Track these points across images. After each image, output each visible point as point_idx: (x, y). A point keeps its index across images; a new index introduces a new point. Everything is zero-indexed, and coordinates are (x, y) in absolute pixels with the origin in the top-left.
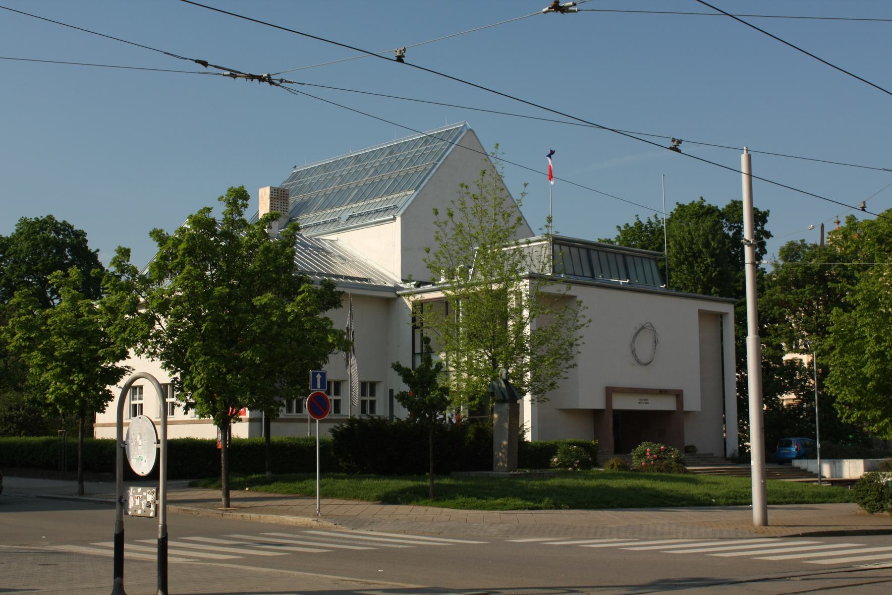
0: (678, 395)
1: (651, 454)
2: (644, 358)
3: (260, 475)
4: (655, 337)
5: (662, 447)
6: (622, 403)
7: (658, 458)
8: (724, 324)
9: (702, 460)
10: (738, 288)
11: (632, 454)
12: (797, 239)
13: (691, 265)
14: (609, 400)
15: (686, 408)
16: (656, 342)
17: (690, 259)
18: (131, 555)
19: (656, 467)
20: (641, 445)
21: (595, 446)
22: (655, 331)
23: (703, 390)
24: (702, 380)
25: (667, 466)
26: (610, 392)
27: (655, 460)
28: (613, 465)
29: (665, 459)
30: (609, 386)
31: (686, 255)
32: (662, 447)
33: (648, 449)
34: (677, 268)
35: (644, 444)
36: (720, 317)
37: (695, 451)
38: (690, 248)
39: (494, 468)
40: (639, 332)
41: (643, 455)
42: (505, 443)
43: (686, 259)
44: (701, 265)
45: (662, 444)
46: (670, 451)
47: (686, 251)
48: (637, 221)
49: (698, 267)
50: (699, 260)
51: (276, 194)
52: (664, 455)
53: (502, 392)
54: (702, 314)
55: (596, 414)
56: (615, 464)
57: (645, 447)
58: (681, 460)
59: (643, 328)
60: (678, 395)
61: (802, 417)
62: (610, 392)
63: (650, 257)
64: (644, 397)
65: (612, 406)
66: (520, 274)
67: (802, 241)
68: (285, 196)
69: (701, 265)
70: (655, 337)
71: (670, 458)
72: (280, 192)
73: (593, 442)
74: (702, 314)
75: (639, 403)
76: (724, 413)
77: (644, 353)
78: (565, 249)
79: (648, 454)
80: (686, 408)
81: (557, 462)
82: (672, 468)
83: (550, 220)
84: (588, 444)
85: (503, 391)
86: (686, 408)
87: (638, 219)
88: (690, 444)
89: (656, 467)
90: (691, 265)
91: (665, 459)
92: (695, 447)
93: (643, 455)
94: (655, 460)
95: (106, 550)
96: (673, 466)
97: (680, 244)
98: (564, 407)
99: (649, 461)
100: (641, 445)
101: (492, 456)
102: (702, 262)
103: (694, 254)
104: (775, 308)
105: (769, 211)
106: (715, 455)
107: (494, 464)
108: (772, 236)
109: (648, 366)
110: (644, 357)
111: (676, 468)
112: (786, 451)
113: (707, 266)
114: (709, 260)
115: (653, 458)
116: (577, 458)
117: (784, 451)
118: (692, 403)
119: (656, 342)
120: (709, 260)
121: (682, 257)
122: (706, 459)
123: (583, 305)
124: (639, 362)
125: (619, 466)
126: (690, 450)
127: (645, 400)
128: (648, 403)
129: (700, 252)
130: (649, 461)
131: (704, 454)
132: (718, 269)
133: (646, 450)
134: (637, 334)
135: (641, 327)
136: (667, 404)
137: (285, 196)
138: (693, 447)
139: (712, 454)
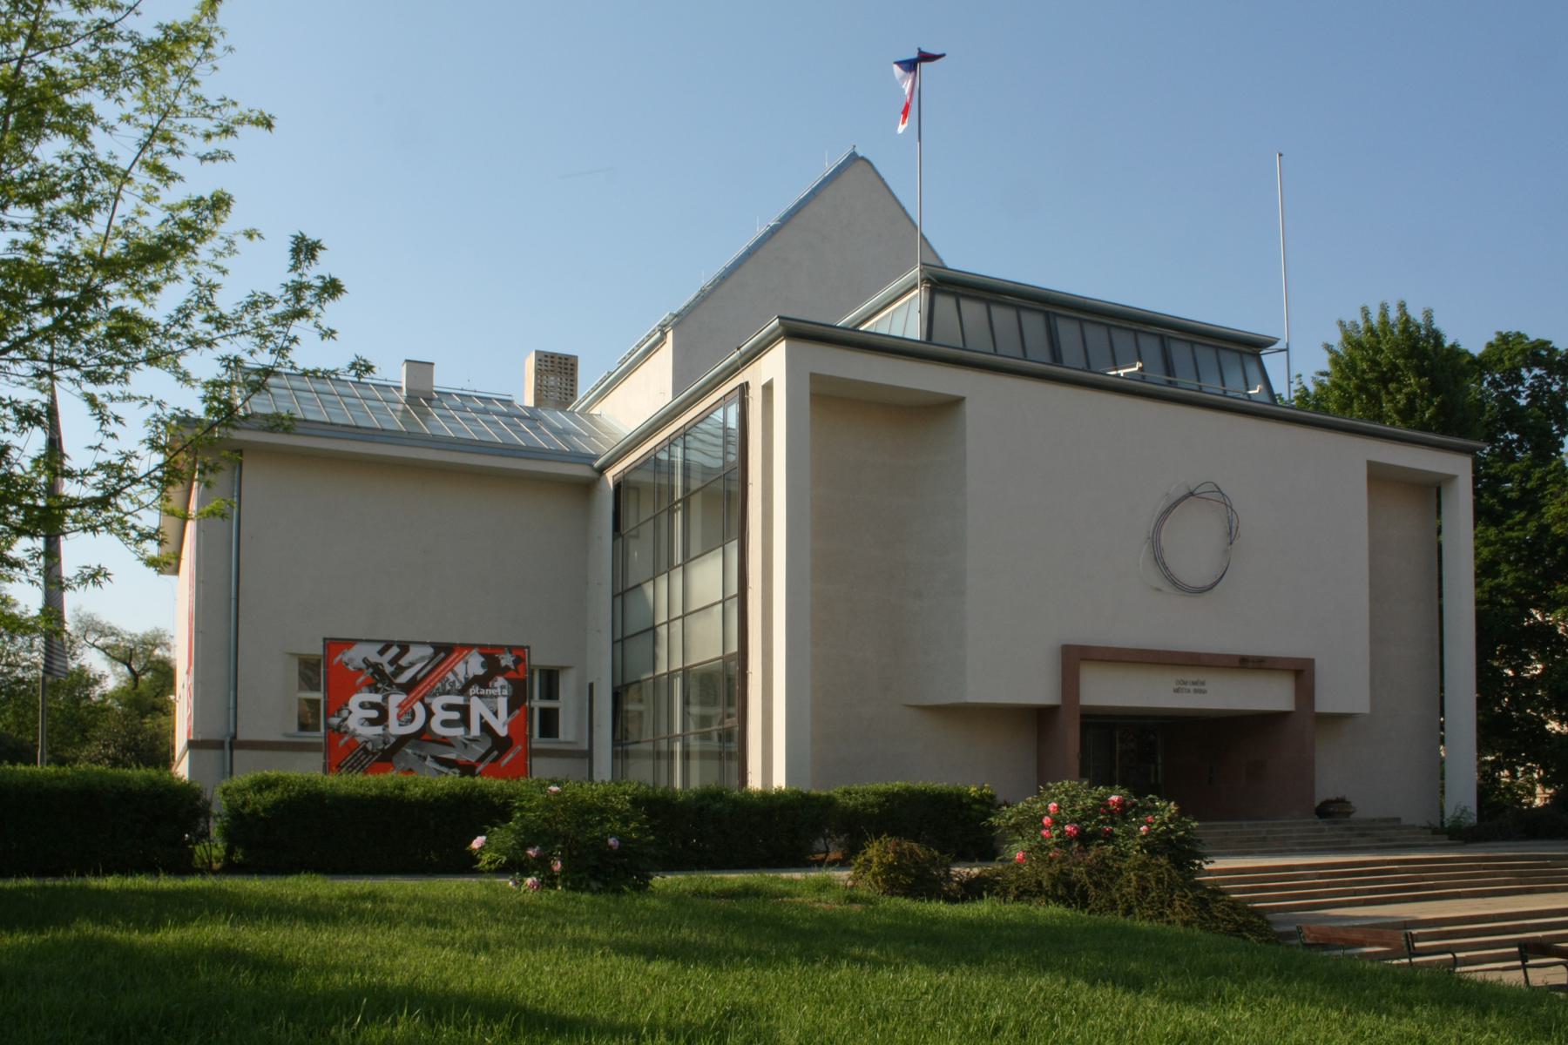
0: (1301, 673)
1: (1057, 822)
3: (117, 936)
4: (1230, 522)
9: (1363, 835)
10: (1509, 495)
15: (1324, 704)
16: (1231, 534)
17: (1373, 387)
22: (1228, 506)
24: (1376, 639)
26: (1074, 659)
36: (1433, 490)
37: (1348, 814)
43: (1361, 388)
47: (1364, 372)
50: (1392, 386)
51: (549, 364)
55: (1040, 719)
60: (1301, 673)
62: (1074, 659)
64: (1191, 676)
65: (1077, 695)
68: (569, 367)
70: (1230, 522)
72: (557, 361)
74: (1379, 476)
75: (1176, 691)
76: (1442, 714)
77: (1194, 563)
79: (1046, 820)
80: (1325, 703)
86: (1325, 703)
88: (1332, 796)
90: (1375, 399)
98: (927, 703)
109: (1207, 595)
113: (1411, 398)
119: (1231, 534)
121: (1354, 381)
124: (1175, 583)
127: (1195, 683)
128: (1204, 692)
129: (1395, 367)
132: (1436, 401)
134: (1166, 513)
135: (1187, 491)
136: (1273, 695)
137: (569, 367)
138: (1341, 801)
139: (1398, 819)
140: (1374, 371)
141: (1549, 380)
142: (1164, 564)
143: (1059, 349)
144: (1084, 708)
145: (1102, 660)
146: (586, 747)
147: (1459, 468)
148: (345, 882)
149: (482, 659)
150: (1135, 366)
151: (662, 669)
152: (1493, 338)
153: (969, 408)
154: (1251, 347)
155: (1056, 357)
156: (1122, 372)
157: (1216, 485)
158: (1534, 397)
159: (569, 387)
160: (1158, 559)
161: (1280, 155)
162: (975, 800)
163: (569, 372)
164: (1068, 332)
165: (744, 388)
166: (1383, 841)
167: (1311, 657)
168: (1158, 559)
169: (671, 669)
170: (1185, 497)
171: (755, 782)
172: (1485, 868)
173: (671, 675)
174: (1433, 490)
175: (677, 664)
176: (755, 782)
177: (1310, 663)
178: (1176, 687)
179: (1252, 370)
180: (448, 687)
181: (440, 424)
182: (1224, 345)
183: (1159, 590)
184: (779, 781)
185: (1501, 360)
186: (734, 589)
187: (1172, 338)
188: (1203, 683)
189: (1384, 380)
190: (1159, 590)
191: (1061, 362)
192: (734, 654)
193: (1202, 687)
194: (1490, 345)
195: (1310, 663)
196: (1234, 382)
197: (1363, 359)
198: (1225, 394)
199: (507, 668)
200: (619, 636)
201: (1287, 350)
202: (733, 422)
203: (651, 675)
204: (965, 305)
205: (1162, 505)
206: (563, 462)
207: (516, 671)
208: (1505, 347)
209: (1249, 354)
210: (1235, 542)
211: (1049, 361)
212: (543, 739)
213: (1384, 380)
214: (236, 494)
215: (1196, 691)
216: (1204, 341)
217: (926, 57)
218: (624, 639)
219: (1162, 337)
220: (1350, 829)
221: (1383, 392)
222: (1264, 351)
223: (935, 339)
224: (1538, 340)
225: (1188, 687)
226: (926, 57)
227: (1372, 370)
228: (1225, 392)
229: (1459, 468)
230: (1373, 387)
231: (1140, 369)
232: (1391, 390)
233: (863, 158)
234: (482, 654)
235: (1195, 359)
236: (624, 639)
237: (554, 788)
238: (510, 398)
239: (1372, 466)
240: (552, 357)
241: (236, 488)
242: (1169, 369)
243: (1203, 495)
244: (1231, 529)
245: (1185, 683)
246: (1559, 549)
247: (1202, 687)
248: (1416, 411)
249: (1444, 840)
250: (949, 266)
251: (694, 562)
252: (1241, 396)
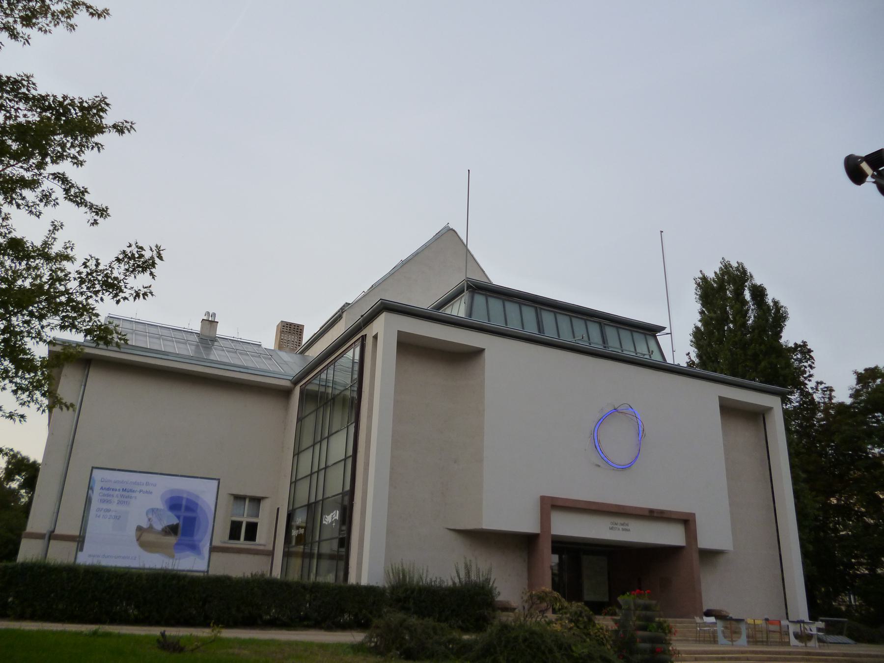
0: (687, 522)
14: (545, 520)
16: (641, 434)
48: (689, 360)
51: (288, 328)
60: (687, 522)
61: (855, 424)
64: (619, 521)
66: (23, 95)
74: (728, 409)
75: (611, 529)
77: (620, 450)
80: (705, 541)
87: (690, 359)
95: (873, 653)
108: (856, 372)
135: (612, 408)
136: (672, 536)
137: (299, 331)
144: (553, 536)
146: (271, 548)
147: (773, 402)
148: (111, 631)
153: (487, 354)
154: (651, 331)
155: (540, 329)
159: (298, 342)
160: (597, 446)
163: (299, 333)
165: (364, 338)
167: (693, 512)
168: (597, 446)
169: (317, 500)
170: (610, 414)
176: (352, 580)
178: (611, 526)
179: (652, 344)
181: (216, 355)
182: (636, 330)
183: (599, 466)
186: (350, 452)
187: (605, 324)
188: (627, 525)
190: (599, 466)
192: (348, 491)
196: (642, 349)
200: (294, 479)
201: (671, 334)
202: (357, 357)
206: (157, 350)
209: (650, 335)
212: (232, 541)
214: (83, 384)
215: (623, 530)
216: (640, 331)
218: (295, 482)
222: (658, 334)
225: (618, 526)
233: (452, 230)
236: (295, 482)
238: (260, 344)
239: (721, 398)
240: (290, 325)
242: (604, 341)
243: (625, 411)
250: (494, 283)
251: (334, 436)
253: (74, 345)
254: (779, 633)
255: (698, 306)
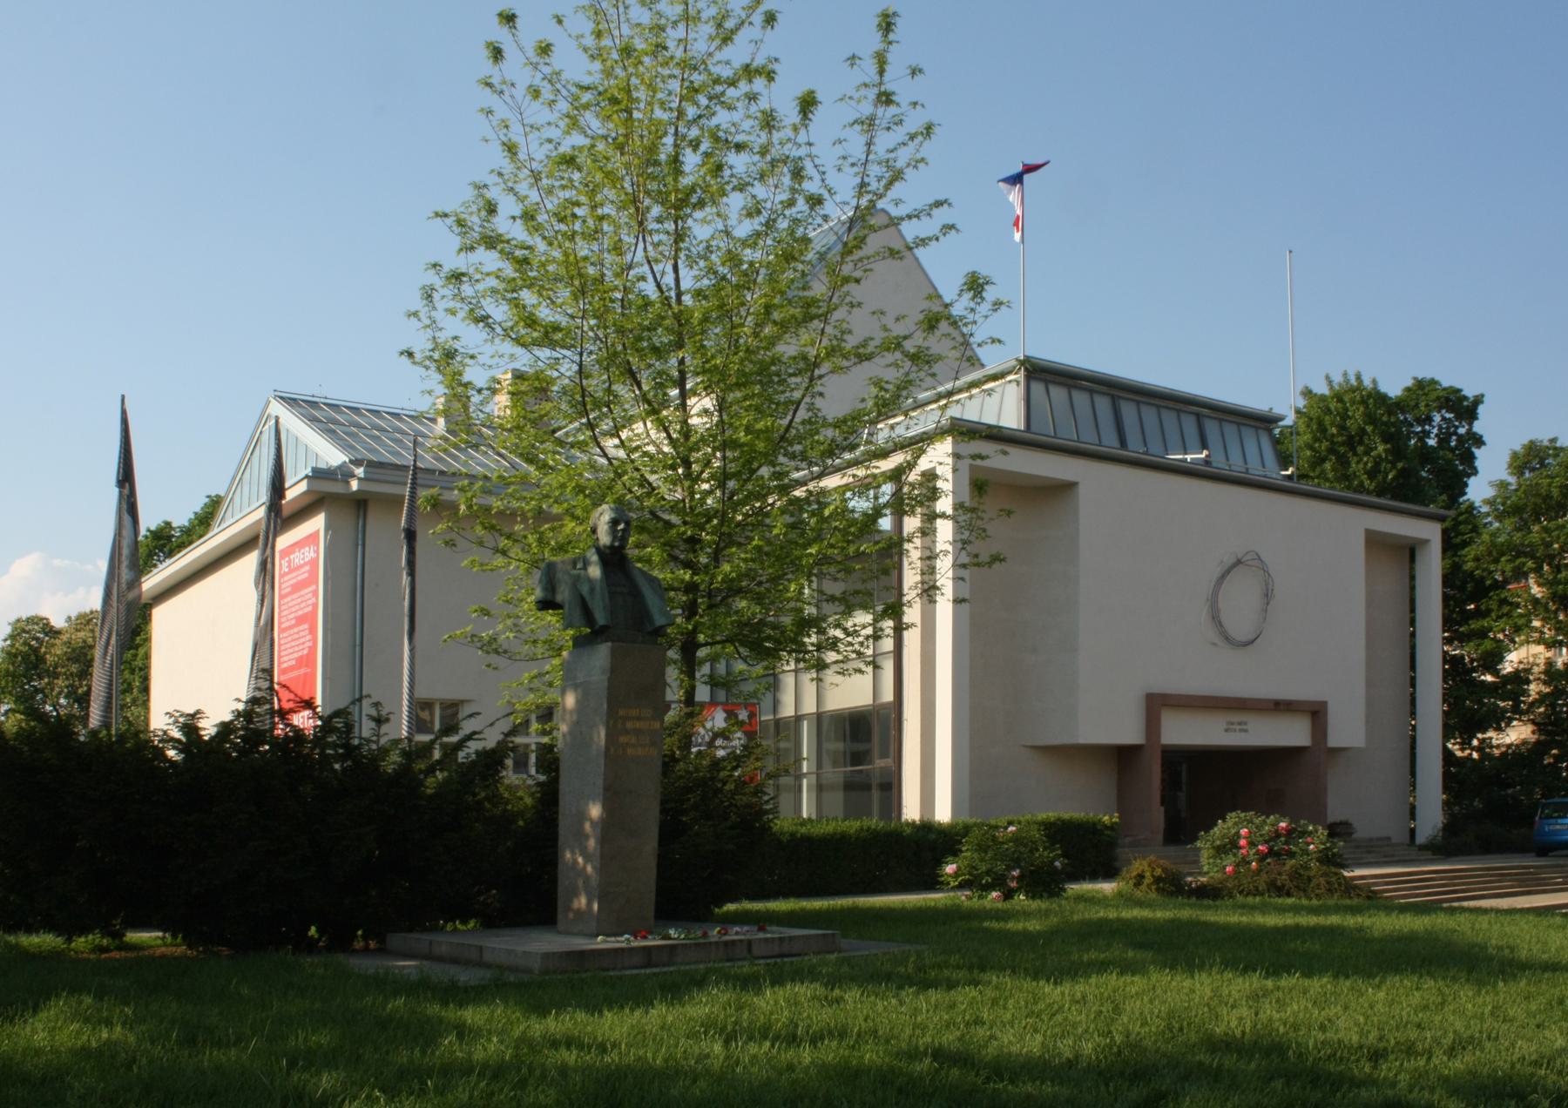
0: (1317, 713)
1: (1252, 844)
2: (1240, 630)
4: (1267, 585)
5: (1283, 825)
6: (1183, 731)
7: (1271, 853)
8: (1418, 558)
9: (1369, 852)
11: (1198, 844)
12: (1543, 436)
13: (1343, 462)
14: (1152, 724)
16: (1268, 595)
17: (1342, 449)
18: (903, 901)
19: (1264, 877)
20: (1224, 820)
21: (1112, 827)
23: (1370, 704)
25: (1295, 875)
26: (1156, 705)
27: (1262, 858)
28: (1141, 877)
29: (1291, 855)
30: (1151, 691)
31: (1332, 443)
32: (1283, 825)
33: (1244, 831)
34: (1314, 471)
35: (1232, 817)
36: (1410, 551)
37: (1351, 834)
38: (1342, 428)
39: (560, 916)
40: (1228, 571)
41: (1229, 846)
42: (595, 811)
43: (1331, 451)
44: (1365, 459)
45: (1283, 815)
46: (1304, 833)
47: (1333, 435)
49: (1358, 462)
52: (1287, 843)
53: (583, 599)
54: (1375, 541)
55: (1123, 757)
56: (1148, 874)
57: (1236, 825)
58: (1334, 855)
59: (1239, 562)
60: (1317, 713)
62: (1156, 705)
63: (1258, 424)
64: (1236, 717)
65: (1159, 736)
67: (1553, 440)
69: (1365, 459)
70: (1267, 585)
71: (1306, 852)
73: (1106, 818)
74: (1375, 541)
75: (1227, 730)
77: (1240, 621)
78: (1059, 393)
79: (1242, 842)
80: (1334, 741)
81: (956, 875)
82: (1309, 879)
83: (887, 24)
84: (1094, 824)
85: (585, 590)
86: (1334, 741)
89: (1264, 877)
90: (1343, 462)
91: (1291, 855)
92: (1351, 825)
93: (1229, 846)
94: (1262, 858)
96: (1312, 873)
97: (1320, 423)
99: (1245, 862)
100: (1224, 820)
101: (555, 865)
102: (1367, 453)
103: (1350, 437)
104: (1503, 559)
105: (1483, 396)
106: (1394, 841)
107: (560, 903)
109: (1250, 647)
110: (1240, 626)
111: (1322, 880)
112: (1558, 827)
114: (1381, 448)
115: (1258, 852)
116: (1016, 862)
117: (1551, 827)
118: (1347, 730)
119: (1268, 595)
120: (1381, 448)
121: (1325, 444)
122: (1377, 851)
123: (990, 293)
124: (1227, 638)
125: (1157, 880)
126: (1338, 830)
128: (1246, 731)
130: (1245, 862)
131: (1371, 840)
132: (1400, 465)
133: (1238, 834)
136: (1292, 733)
139: (1389, 838)
140: (1342, 435)
141: (1457, 423)
142: (1220, 622)
143: (1123, 428)
144: (1164, 746)
145: (1179, 706)
149: (725, 715)
150: (1202, 453)
151: (788, 711)
152: (1409, 383)
153: (1082, 490)
155: (1123, 443)
156: (1189, 457)
157: (1257, 554)
158: (1443, 440)
161: (1290, 252)
162: (1106, 827)
164: (1128, 411)
166: (1385, 856)
167: (1324, 700)
171: (911, 811)
172: (1492, 876)
173: (798, 719)
174: (1410, 551)
175: (809, 707)
176: (911, 811)
177: (1324, 704)
180: (700, 740)
183: (1214, 644)
184: (943, 813)
185: (1417, 406)
188: (1245, 724)
189: (1351, 443)
190: (1214, 644)
191: (1126, 446)
193: (1244, 727)
194: (1408, 389)
195: (1324, 704)
197: (1332, 424)
198: (1247, 472)
199: (743, 722)
203: (771, 717)
204: (1052, 389)
205: (1218, 572)
207: (750, 724)
208: (1421, 392)
210: (1271, 602)
211: (1119, 446)
213: (1351, 443)
215: (1241, 730)
217: (1030, 169)
219: (1198, 415)
220: (1357, 847)
221: (1350, 454)
223: (1033, 429)
224: (1451, 387)
225: (1234, 727)
226: (1030, 169)
227: (1340, 434)
228: (1247, 469)
229: (1431, 532)
230: (1342, 449)
231: (1207, 456)
232: (1359, 452)
234: (725, 711)
235: (1223, 435)
237: (1012, 828)
241: (360, 536)
243: (1249, 563)
244: (1267, 590)
245: (1232, 724)
246: (1469, 585)
247: (1244, 727)
248: (1380, 472)
249: (1428, 855)
252: (1274, 476)
253: (1446, 611)
254: (799, 674)
255: (1446, 383)
